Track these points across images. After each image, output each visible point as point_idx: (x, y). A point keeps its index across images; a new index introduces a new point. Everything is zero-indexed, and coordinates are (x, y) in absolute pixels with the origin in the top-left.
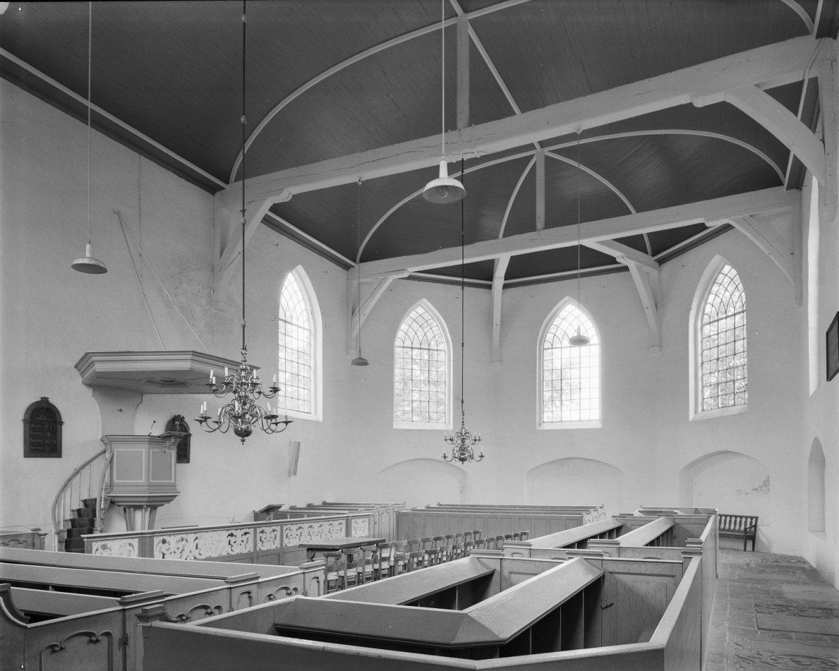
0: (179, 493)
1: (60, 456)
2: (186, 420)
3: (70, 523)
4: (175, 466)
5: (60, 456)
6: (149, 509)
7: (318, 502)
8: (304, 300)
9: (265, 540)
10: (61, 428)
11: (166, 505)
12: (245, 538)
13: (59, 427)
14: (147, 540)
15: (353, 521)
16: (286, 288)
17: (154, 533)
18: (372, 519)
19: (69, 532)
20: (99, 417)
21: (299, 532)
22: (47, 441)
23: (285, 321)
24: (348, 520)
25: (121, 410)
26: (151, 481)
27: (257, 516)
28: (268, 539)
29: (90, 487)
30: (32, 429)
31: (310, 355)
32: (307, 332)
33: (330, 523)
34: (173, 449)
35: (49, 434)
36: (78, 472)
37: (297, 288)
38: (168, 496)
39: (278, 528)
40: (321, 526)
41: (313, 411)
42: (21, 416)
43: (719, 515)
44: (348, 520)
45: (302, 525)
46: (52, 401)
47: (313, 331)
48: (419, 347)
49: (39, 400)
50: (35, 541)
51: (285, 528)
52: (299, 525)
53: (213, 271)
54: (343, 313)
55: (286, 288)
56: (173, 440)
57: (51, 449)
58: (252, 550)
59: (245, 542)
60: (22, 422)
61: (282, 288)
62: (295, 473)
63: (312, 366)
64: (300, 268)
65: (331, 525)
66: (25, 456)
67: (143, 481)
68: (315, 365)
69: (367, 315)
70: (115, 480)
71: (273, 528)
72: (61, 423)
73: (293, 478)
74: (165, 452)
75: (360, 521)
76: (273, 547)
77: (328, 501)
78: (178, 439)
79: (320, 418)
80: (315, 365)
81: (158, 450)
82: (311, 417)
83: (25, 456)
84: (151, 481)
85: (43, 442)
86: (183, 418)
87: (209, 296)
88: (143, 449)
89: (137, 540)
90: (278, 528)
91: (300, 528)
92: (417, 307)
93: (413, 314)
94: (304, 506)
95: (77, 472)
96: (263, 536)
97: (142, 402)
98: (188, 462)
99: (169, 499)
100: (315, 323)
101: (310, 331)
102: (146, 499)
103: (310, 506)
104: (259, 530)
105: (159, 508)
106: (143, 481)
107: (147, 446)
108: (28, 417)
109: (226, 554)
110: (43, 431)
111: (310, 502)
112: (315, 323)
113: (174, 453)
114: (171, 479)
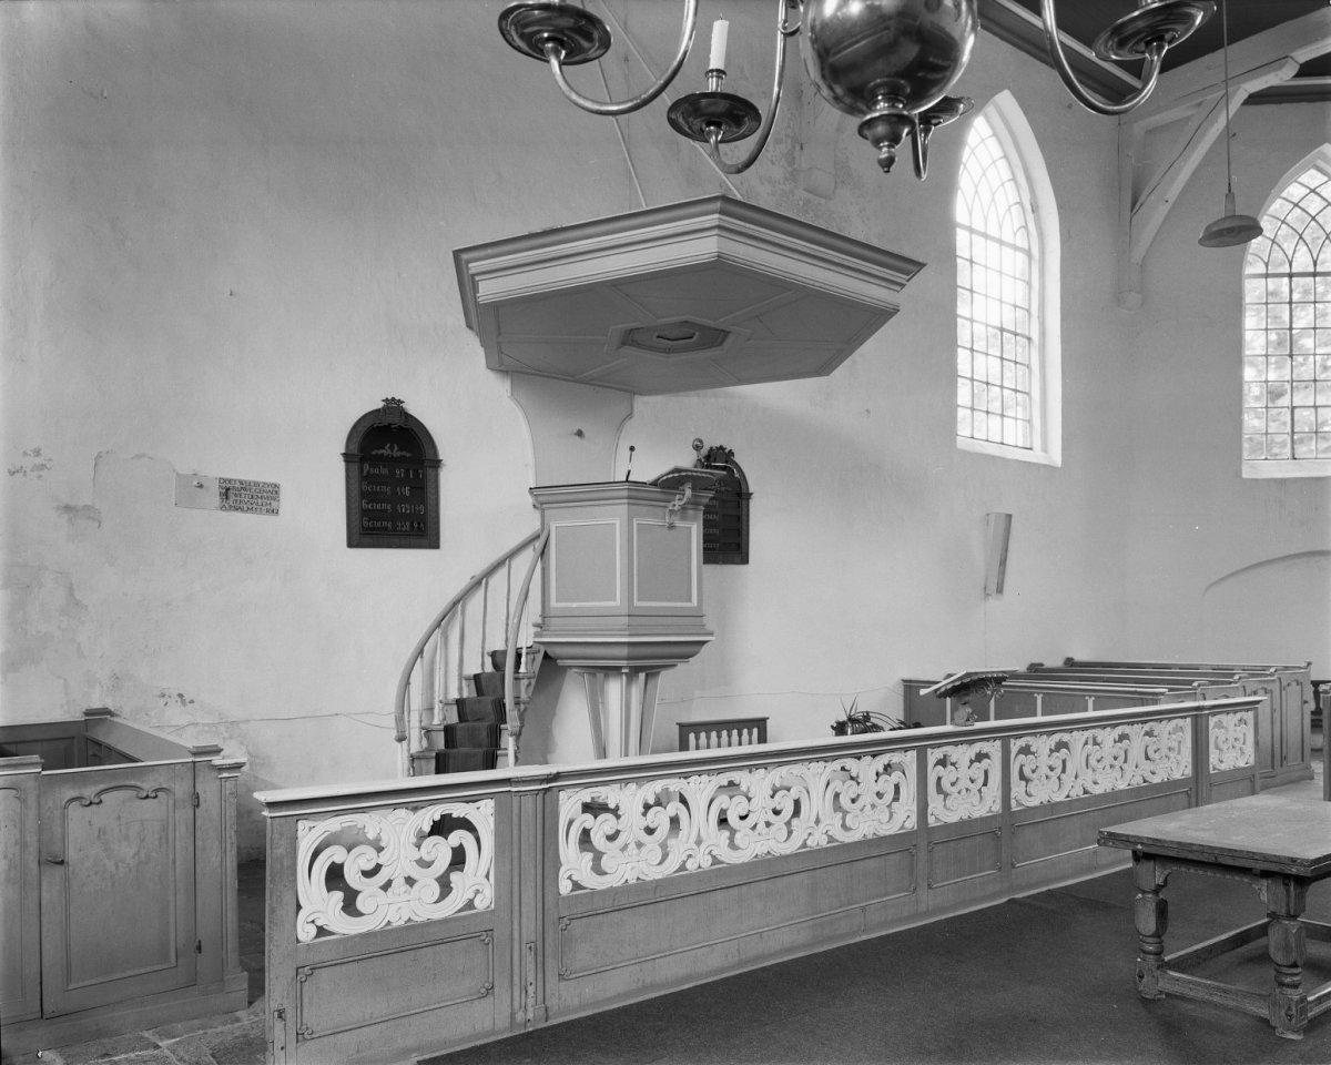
0: (711, 634)
1: (435, 545)
2: (737, 459)
3: (455, 708)
4: (699, 568)
5: (435, 545)
6: (642, 676)
7: (1054, 661)
8: (1014, 179)
9: (954, 790)
10: (437, 476)
11: (681, 667)
12: (887, 784)
13: (430, 471)
14: (528, 802)
15: (1213, 721)
16: (973, 152)
17: (557, 777)
18: (1264, 710)
19: (449, 731)
20: (530, 451)
21: (1056, 761)
22: (404, 508)
23: (971, 230)
24: (1199, 718)
25: (580, 434)
26: (636, 603)
27: (918, 703)
28: (964, 783)
29: (497, 626)
30: (366, 478)
31: (1028, 311)
32: (1021, 257)
33: (1147, 727)
34: (695, 519)
35: (407, 492)
36: (479, 583)
37: (997, 152)
38: (1080, 690)
39: (994, 748)
40: (1123, 737)
41: (1037, 444)
42: (340, 447)
43: (1312, 682)
44: (1199, 718)
45: (1066, 737)
46: (413, 408)
47: (1035, 252)
48: (1311, 270)
49: (380, 405)
50: (199, 789)
51: (1015, 745)
52: (1056, 737)
53: (799, 98)
54: (1106, 202)
55: (973, 152)
56: (688, 492)
57: (412, 526)
58: (912, 824)
59: (889, 796)
60: (342, 458)
61: (959, 168)
62: (1000, 590)
63: (1035, 337)
64: (1005, 99)
65: (1149, 734)
66: (350, 545)
67: (617, 602)
68: (1043, 334)
69: (1171, 201)
70: (553, 603)
71: (977, 747)
72: (436, 463)
73: (994, 603)
74: (671, 527)
75: (1230, 720)
76: (980, 812)
77: (1081, 655)
78: (720, 509)
79: (1056, 458)
80: (1043, 334)
81: (651, 521)
82: (1036, 457)
83: (350, 545)
84: (636, 603)
85: (394, 508)
86: (731, 453)
87: (791, 159)
88: (614, 519)
89: (488, 806)
90: (994, 748)
91: (1061, 745)
92: (1305, 169)
93: (1294, 191)
94: (1021, 668)
95: (477, 583)
96: (948, 775)
97: (630, 416)
98: (745, 560)
99: (685, 651)
100: (1041, 235)
101: (1029, 253)
102: (624, 651)
103: (1036, 671)
104: (933, 756)
105: (664, 674)
106: (618, 603)
107: (622, 509)
108: (355, 449)
109: (824, 842)
110: (392, 479)
111: (1036, 661)
112: (1041, 235)
113: (694, 532)
114: (690, 600)
